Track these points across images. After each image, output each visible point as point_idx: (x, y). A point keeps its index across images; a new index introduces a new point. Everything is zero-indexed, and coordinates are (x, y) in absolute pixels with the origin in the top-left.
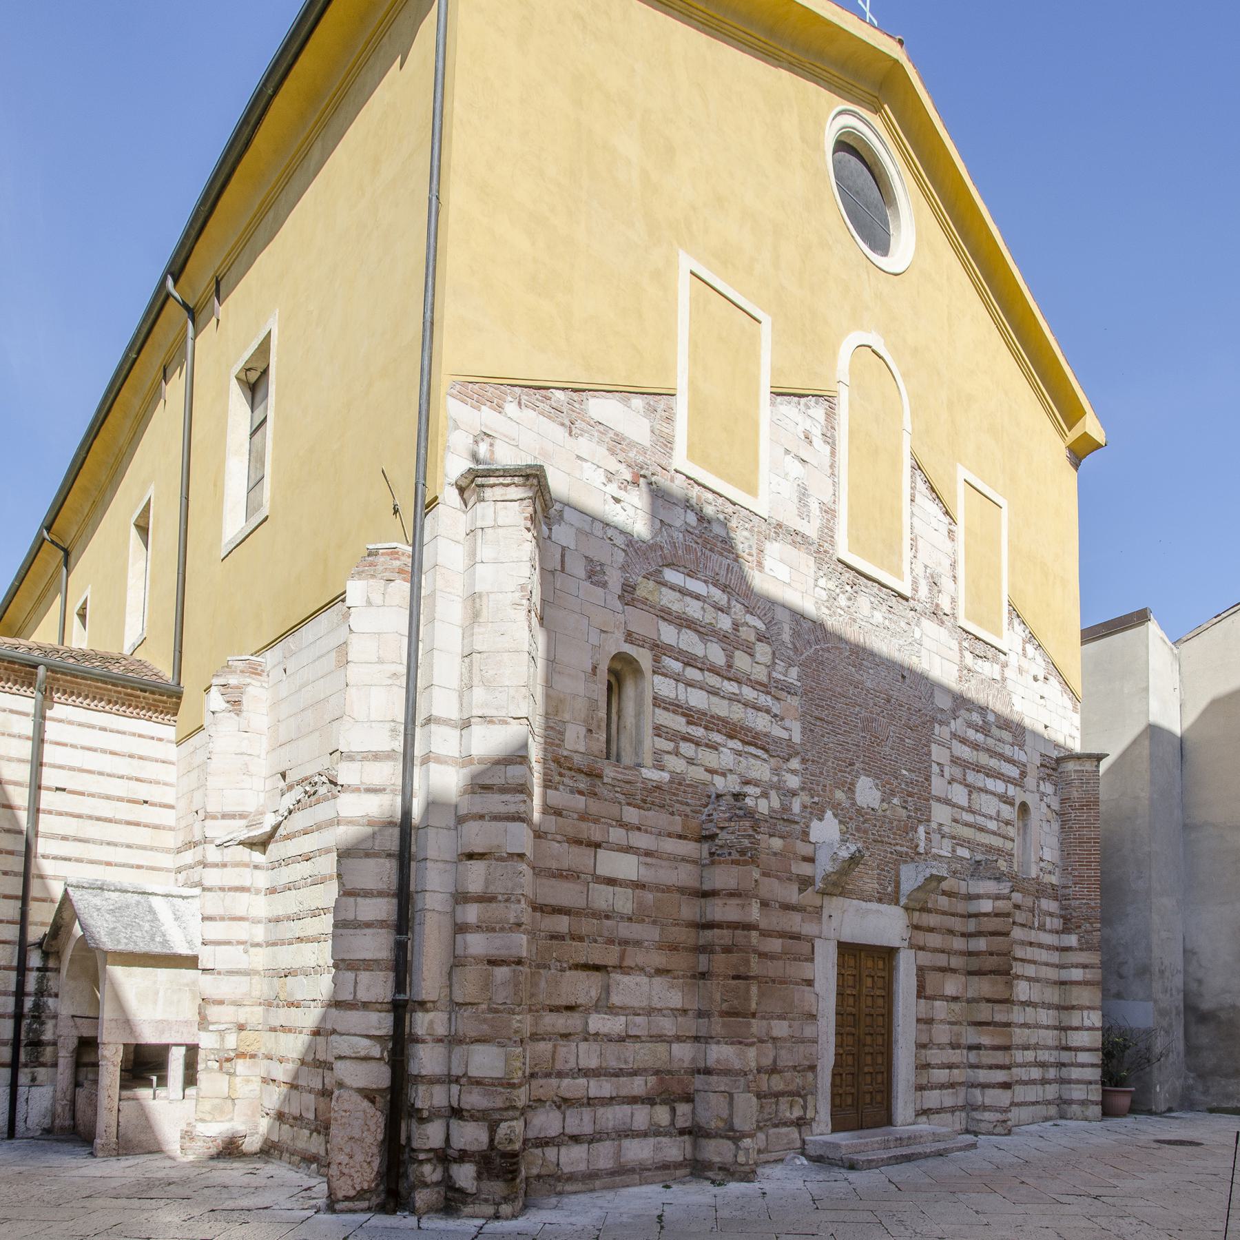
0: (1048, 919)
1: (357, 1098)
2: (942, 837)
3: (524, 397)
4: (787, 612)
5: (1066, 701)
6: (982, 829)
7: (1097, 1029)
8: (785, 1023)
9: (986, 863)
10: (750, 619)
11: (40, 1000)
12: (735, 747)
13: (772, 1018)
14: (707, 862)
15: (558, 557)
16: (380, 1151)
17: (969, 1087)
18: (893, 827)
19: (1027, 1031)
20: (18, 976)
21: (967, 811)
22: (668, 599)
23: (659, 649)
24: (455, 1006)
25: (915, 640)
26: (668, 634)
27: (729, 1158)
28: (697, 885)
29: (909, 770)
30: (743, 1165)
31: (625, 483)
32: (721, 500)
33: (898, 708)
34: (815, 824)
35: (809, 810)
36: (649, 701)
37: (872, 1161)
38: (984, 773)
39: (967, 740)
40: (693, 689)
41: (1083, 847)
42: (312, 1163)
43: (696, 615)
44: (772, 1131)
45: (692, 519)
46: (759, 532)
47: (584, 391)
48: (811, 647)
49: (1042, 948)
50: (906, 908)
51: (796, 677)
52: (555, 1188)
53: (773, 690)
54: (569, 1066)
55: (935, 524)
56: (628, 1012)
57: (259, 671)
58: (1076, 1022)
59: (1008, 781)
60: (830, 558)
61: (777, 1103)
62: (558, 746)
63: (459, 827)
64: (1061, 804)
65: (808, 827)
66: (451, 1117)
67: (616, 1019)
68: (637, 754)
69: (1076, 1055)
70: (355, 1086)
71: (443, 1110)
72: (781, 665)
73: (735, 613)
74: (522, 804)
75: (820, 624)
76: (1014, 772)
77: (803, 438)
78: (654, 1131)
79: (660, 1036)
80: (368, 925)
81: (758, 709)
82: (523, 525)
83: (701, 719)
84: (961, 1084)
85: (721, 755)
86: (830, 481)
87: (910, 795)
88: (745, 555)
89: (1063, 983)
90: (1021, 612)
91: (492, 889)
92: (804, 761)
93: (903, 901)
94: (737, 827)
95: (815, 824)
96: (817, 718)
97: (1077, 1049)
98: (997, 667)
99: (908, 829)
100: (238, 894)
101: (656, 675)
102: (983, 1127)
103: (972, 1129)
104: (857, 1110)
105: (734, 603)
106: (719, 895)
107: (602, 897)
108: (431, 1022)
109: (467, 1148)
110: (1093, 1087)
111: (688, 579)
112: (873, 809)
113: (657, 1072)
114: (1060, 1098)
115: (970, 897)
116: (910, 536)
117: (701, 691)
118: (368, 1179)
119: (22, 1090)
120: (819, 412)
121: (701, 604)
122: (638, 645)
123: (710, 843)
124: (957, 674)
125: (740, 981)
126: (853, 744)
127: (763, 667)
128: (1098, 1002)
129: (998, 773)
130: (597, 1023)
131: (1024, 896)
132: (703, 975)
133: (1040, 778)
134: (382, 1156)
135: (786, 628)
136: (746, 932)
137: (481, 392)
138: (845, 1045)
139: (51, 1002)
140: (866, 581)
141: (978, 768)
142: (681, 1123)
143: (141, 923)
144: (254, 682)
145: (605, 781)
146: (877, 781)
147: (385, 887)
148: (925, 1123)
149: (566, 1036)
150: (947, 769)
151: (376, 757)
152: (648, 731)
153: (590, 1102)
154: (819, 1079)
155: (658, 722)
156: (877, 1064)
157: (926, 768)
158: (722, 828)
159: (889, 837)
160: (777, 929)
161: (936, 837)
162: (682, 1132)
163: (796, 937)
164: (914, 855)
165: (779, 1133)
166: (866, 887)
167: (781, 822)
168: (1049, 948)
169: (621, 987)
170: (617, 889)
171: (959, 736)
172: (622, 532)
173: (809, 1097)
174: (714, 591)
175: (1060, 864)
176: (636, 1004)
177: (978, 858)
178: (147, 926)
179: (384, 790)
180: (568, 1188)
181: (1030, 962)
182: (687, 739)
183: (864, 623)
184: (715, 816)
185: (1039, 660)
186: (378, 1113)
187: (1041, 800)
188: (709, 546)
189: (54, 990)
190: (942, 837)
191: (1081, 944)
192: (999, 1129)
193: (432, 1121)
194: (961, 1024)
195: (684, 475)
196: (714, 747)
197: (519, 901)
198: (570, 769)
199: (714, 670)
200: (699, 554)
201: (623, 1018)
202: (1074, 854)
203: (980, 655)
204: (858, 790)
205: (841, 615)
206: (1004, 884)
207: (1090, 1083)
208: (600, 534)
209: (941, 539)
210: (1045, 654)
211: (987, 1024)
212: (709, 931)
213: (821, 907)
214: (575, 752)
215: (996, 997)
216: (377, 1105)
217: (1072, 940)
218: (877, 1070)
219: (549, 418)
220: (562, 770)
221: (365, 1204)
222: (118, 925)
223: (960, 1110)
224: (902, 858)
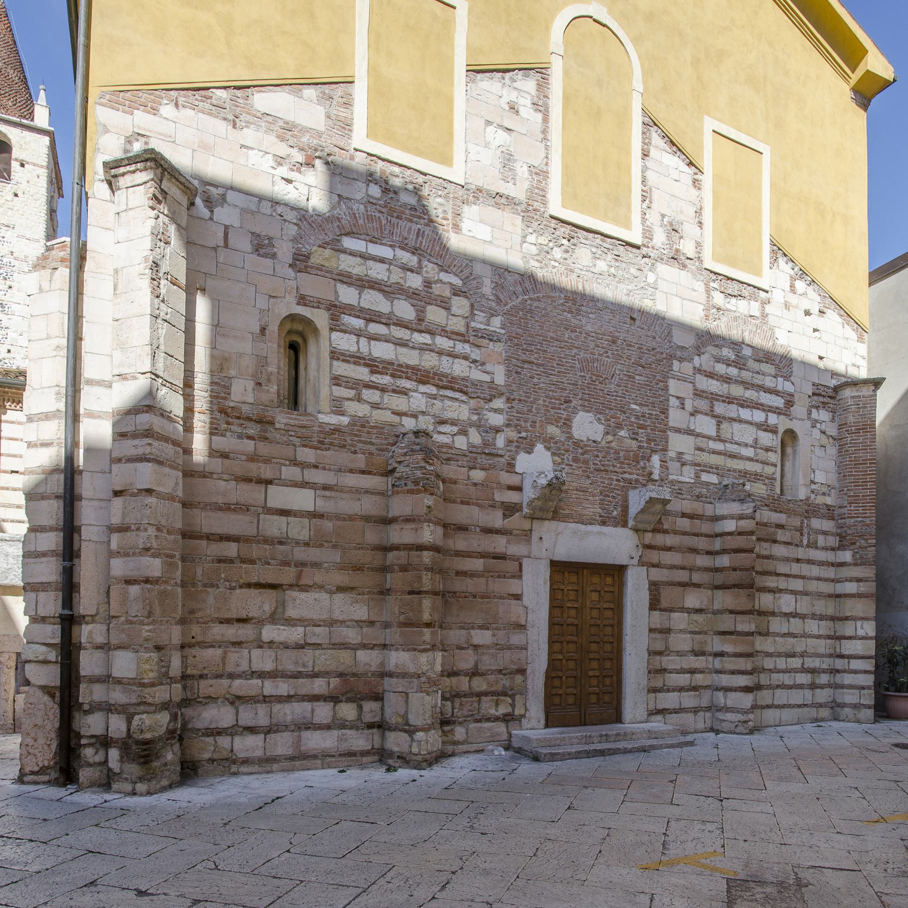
1: (39, 693)
3: (181, 100)
4: (489, 267)
5: (850, 333)
6: (733, 456)
7: (871, 638)
8: (488, 633)
9: (733, 487)
10: (444, 276)
12: (428, 391)
13: (473, 628)
15: (221, 234)
18: (619, 457)
21: (715, 440)
22: (347, 264)
23: (336, 310)
25: (648, 285)
26: (347, 295)
27: (405, 749)
28: (384, 513)
29: (641, 405)
30: (416, 755)
31: (298, 165)
32: (409, 172)
33: (627, 348)
35: (515, 444)
36: (326, 355)
37: (558, 754)
38: (737, 404)
39: (714, 374)
40: (377, 343)
41: (859, 468)
43: (380, 277)
44: (473, 726)
45: (375, 191)
46: (455, 198)
47: (248, 87)
50: (636, 530)
52: (230, 769)
53: (471, 339)
54: (241, 669)
56: (306, 623)
58: (849, 632)
59: (769, 411)
60: (542, 216)
61: (479, 702)
62: (225, 398)
64: (839, 429)
65: (514, 459)
67: (293, 629)
69: (849, 662)
70: (38, 684)
72: (480, 316)
73: (427, 272)
74: (147, 447)
75: (529, 277)
76: (779, 402)
78: (340, 724)
79: (343, 644)
80: (44, 554)
81: (456, 356)
82: (146, 204)
85: (411, 400)
86: (542, 145)
87: (641, 427)
88: (439, 220)
89: (838, 596)
90: (787, 249)
91: (127, 520)
92: (508, 400)
93: (631, 523)
96: (524, 362)
97: (850, 657)
99: (640, 458)
101: (335, 332)
102: (725, 726)
103: (716, 728)
105: (425, 263)
106: (397, 521)
107: (275, 526)
108: (90, 632)
110: (866, 691)
112: (594, 442)
113: (341, 675)
114: (834, 701)
115: (716, 519)
122: (313, 307)
124: (702, 314)
125: (415, 596)
126: (569, 384)
127: (460, 319)
128: (872, 612)
129: (756, 404)
130: (269, 633)
131: (788, 517)
136: (419, 552)
137: (133, 99)
138: (565, 651)
140: (585, 233)
141: (729, 400)
142: (368, 718)
146: (599, 416)
147: (54, 523)
148: (659, 721)
149: (238, 644)
151: (47, 417)
152: (326, 380)
153: (266, 699)
154: (529, 681)
155: (336, 373)
156: (605, 669)
157: (661, 402)
158: (400, 462)
159: (614, 466)
160: (478, 550)
161: (674, 466)
162: (370, 726)
163: (502, 557)
165: (481, 727)
166: (584, 512)
167: (483, 456)
168: (822, 564)
170: (291, 519)
171: (705, 371)
172: (293, 208)
173: (517, 697)
174: (400, 253)
180: (243, 769)
181: (795, 577)
188: (395, 215)
190: (683, 465)
191: (855, 559)
192: (740, 729)
193: (93, 713)
194: (706, 633)
195: (365, 152)
196: (404, 392)
197: (146, 530)
198: (239, 418)
199: (401, 324)
200: (384, 222)
203: (732, 293)
205: (554, 267)
207: (863, 688)
211: (731, 633)
213: (531, 530)
214: (243, 403)
215: (739, 608)
217: (847, 556)
218: (604, 674)
219: (210, 114)
220: (230, 419)
221: (46, 778)
223: (704, 711)
224: (632, 484)
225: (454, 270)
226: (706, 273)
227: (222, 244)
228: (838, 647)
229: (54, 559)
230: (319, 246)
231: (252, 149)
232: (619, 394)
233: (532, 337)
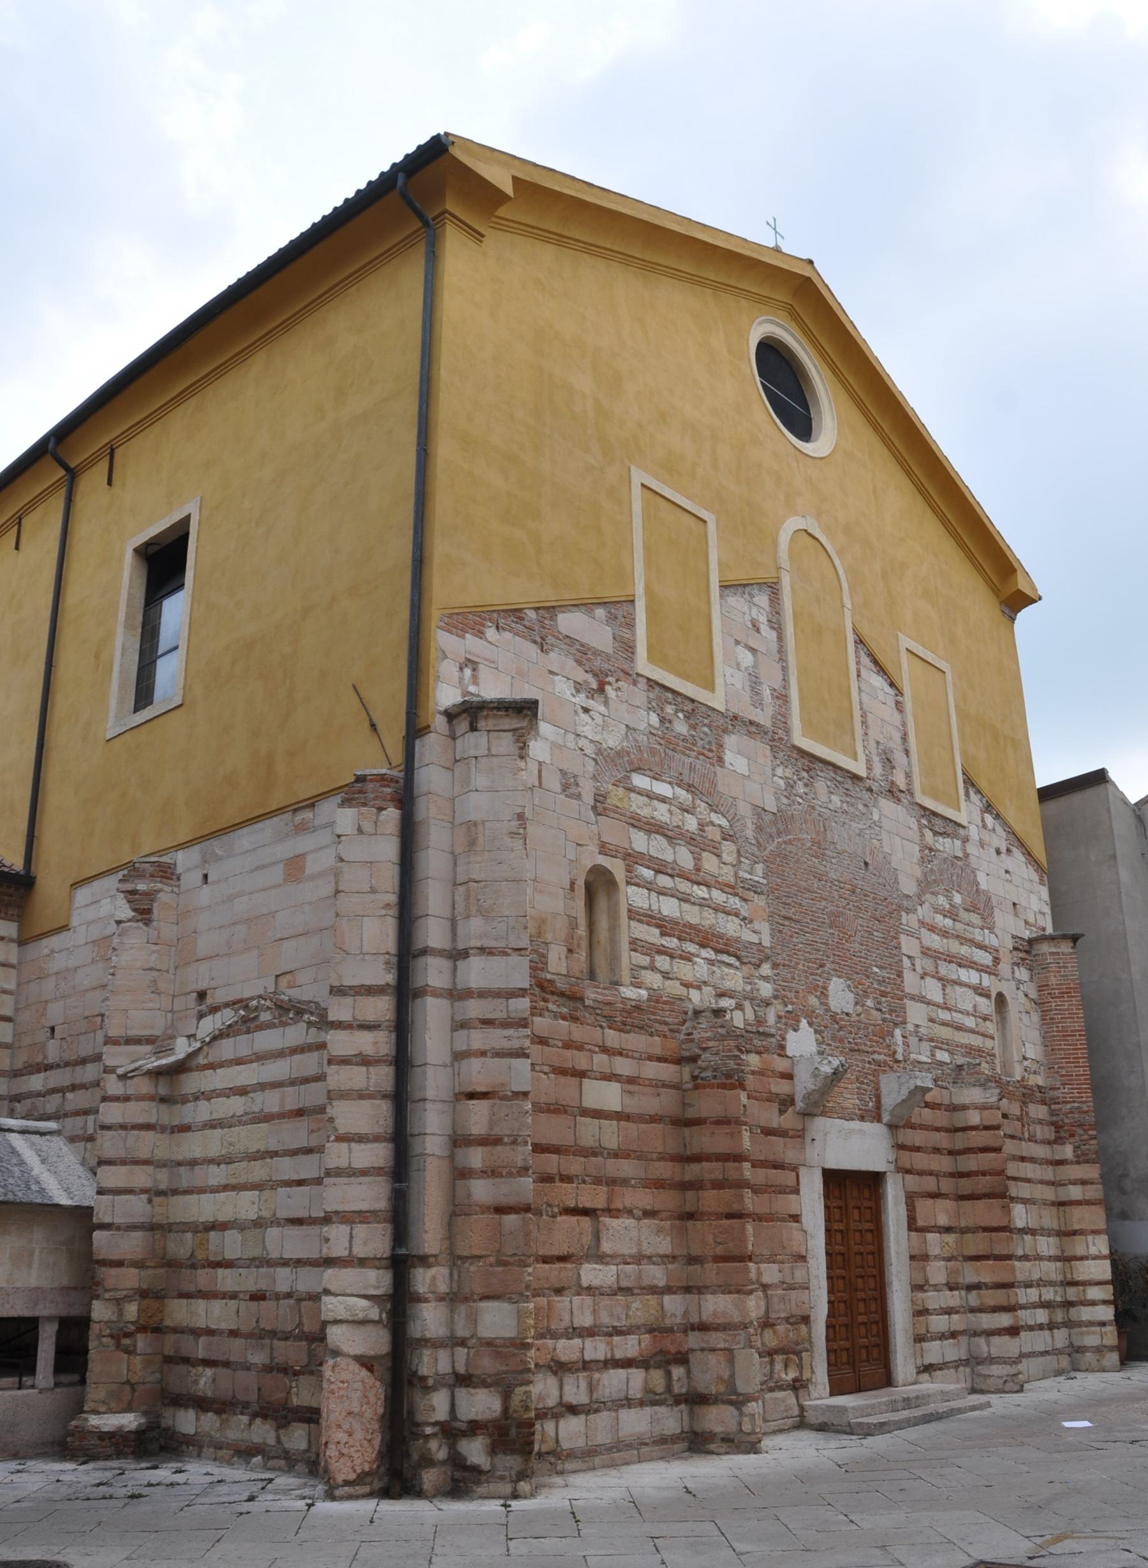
0: (1038, 1128)
1: (355, 1367)
2: (920, 1040)
6: (959, 1028)
9: (968, 1067)
10: (714, 817)
14: (690, 1086)
15: (536, 772)
16: (380, 1427)
17: (971, 1336)
19: (1028, 1264)
21: (942, 1008)
22: (637, 805)
23: (632, 858)
24: (456, 1260)
25: (874, 823)
26: (640, 842)
27: (732, 1427)
29: (880, 967)
34: (791, 1035)
35: (784, 1020)
36: (624, 914)
39: (936, 928)
42: (254, 1456)
43: (663, 819)
44: (768, 1396)
48: (773, 841)
49: (1035, 1163)
51: (761, 875)
52: (556, 1467)
53: (740, 891)
55: (881, 697)
57: (168, 875)
58: (1080, 1251)
59: (982, 970)
62: (542, 970)
63: (456, 1064)
64: (1039, 991)
65: (784, 1039)
66: (454, 1386)
68: (612, 970)
69: (1084, 1291)
70: (352, 1353)
71: (447, 1377)
73: (701, 813)
76: (985, 958)
77: (751, 626)
80: (364, 1172)
81: (728, 913)
82: (517, 754)
83: (674, 928)
84: (963, 1332)
87: (884, 994)
89: (1062, 1204)
91: (497, 1131)
92: (775, 966)
93: (886, 1118)
94: (721, 1047)
95: (791, 1035)
96: (786, 918)
98: (958, 843)
100: (143, 1133)
102: (993, 1383)
104: (854, 1369)
107: (590, 1132)
108: (434, 1278)
109: (479, 1418)
111: (654, 782)
112: (847, 1014)
115: (954, 1108)
116: (860, 712)
117: (673, 899)
118: (369, 1460)
120: (762, 599)
121: (667, 806)
122: (612, 856)
123: (692, 1065)
129: (971, 962)
132: (691, 1216)
133: (1015, 964)
134: (383, 1433)
135: (749, 824)
136: (737, 1164)
141: (950, 959)
145: (586, 1004)
147: (382, 1131)
148: (927, 1382)
150: (918, 962)
151: (371, 991)
152: (625, 946)
159: (865, 1045)
161: (913, 1040)
162: (678, 1400)
164: (894, 1062)
167: (757, 1036)
169: (611, 1232)
171: (927, 924)
173: (804, 1354)
175: (1045, 1061)
176: (626, 1251)
177: (959, 1062)
178: (17, 1174)
179: (379, 1026)
180: (569, 1466)
182: (662, 951)
183: (822, 810)
184: (696, 1036)
185: (999, 829)
186: (378, 1384)
187: (1018, 989)
188: (671, 747)
190: (920, 1040)
191: (1078, 1156)
196: (688, 958)
198: (553, 993)
201: (614, 1268)
202: (1059, 1049)
204: (830, 993)
205: (800, 804)
206: (990, 1091)
208: (571, 745)
209: (888, 712)
210: (1005, 824)
212: (697, 1164)
216: (376, 1374)
217: (1067, 1151)
220: (544, 995)
221: (366, 1489)
223: (963, 1365)
225: (722, 809)
226: (916, 808)
227: (537, 784)
228: (1068, 1271)
230: (614, 785)
231: (557, 674)
232: (863, 955)
233: (789, 887)
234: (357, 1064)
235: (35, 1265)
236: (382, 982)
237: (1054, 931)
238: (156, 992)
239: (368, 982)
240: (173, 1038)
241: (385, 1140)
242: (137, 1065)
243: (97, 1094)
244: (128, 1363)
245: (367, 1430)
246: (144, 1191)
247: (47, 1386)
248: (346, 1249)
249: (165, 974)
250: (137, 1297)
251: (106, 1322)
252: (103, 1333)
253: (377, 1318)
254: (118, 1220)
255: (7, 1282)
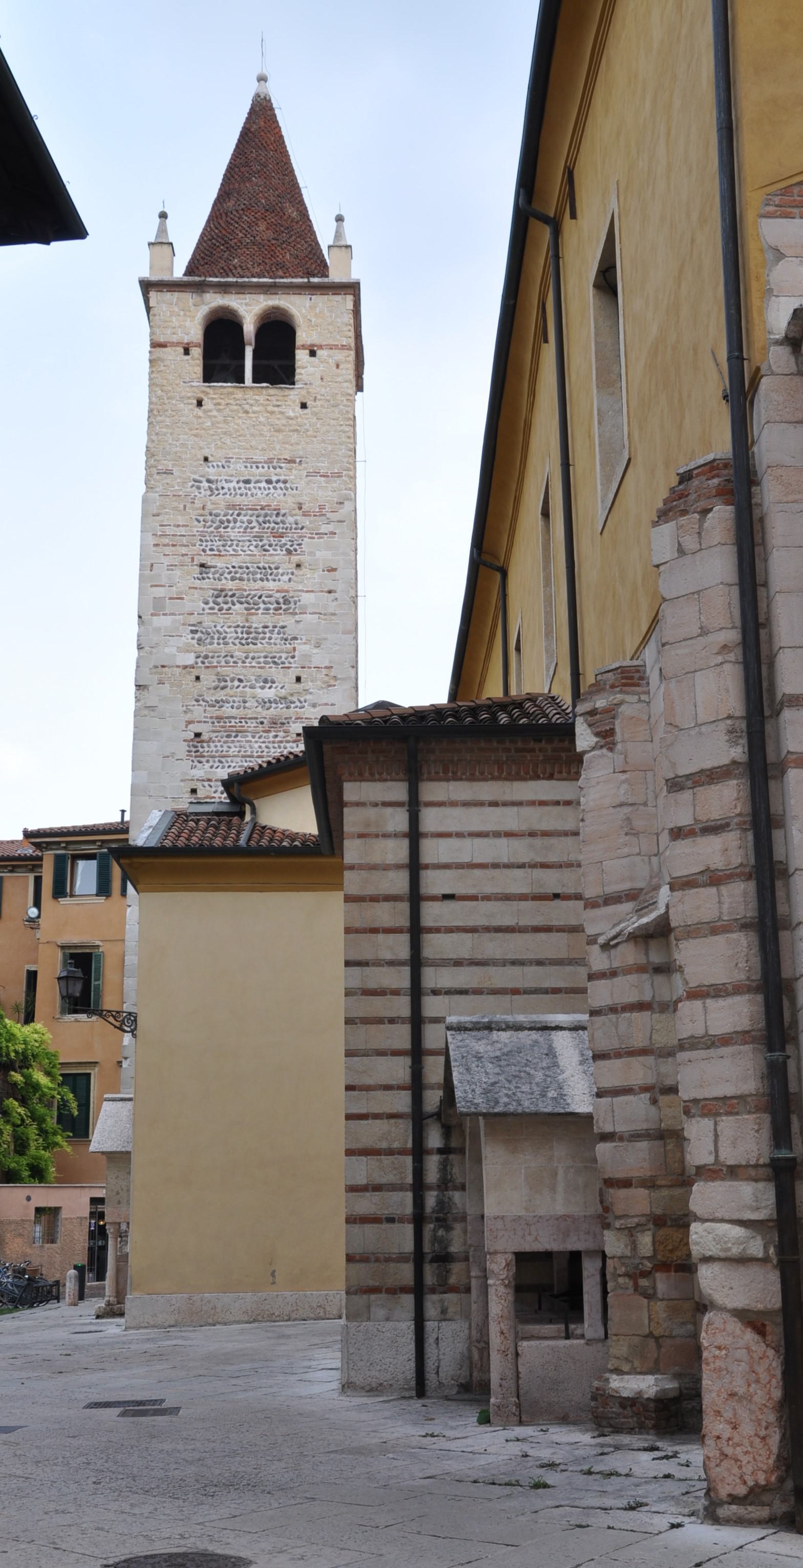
1: (735, 1326)
11: (444, 1195)
16: (779, 1419)
20: (414, 1162)
57: (635, 681)
70: (730, 1305)
80: (725, 1040)
118: (765, 1468)
119: (430, 1325)
139: (457, 1196)
143: (532, 1072)
144: (628, 698)
151: (712, 776)
178: (539, 1076)
179: (728, 825)
186: (771, 1353)
189: (459, 1180)
216: (769, 1338)
221: (764, 1513)
222: (500, 1078)
229: (747, 1048)
234: (704, 886)
235: (561, 1187)
236: (725, 761)
237: (150, 275)
238: (632, 833)
239: (708, 765)
240: (657, 888)
241: (749, 990)
242: (618, 929)
243: (583, 972)
244: (649, 1310)
245: (759, 1421)
246: (646, 1089)
247: (596, 1336)
248: (710, 1153)
249: (642, 807)
250: (652, 1226)
251: (620, 1258)
252: (618, 1272)
253: (760, 1255)
254: (620, 1128)
255: (527, 1209)
